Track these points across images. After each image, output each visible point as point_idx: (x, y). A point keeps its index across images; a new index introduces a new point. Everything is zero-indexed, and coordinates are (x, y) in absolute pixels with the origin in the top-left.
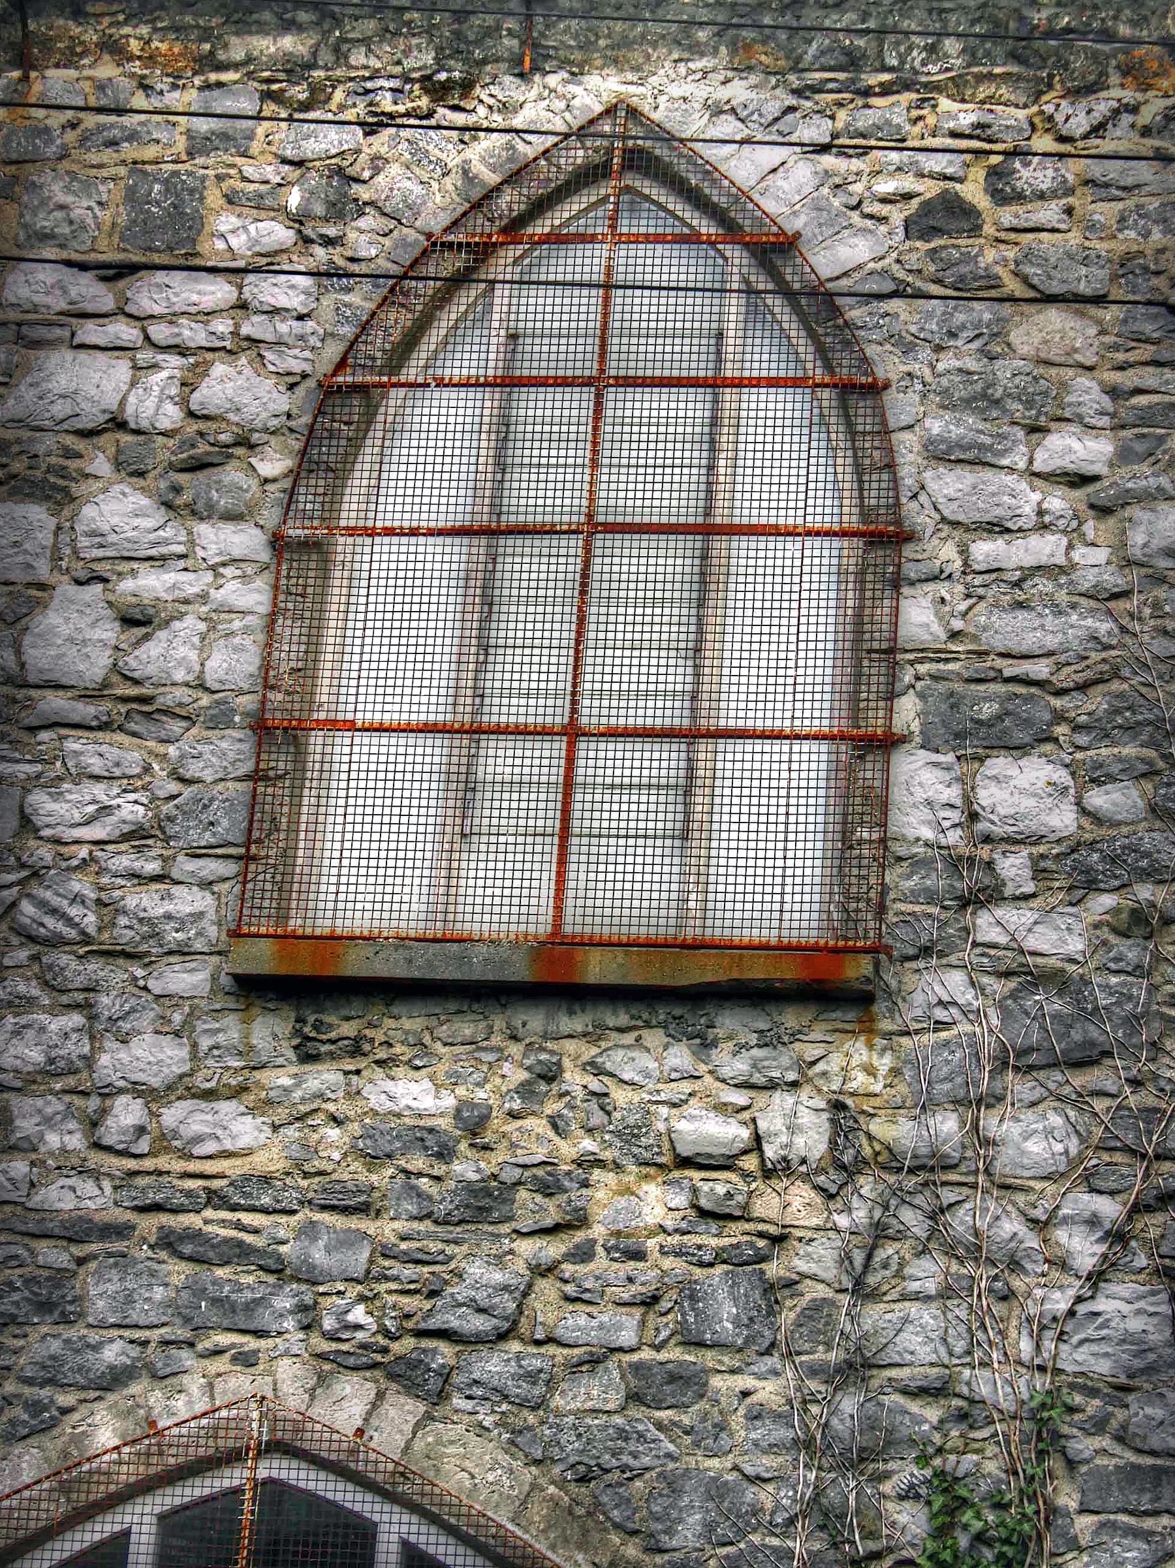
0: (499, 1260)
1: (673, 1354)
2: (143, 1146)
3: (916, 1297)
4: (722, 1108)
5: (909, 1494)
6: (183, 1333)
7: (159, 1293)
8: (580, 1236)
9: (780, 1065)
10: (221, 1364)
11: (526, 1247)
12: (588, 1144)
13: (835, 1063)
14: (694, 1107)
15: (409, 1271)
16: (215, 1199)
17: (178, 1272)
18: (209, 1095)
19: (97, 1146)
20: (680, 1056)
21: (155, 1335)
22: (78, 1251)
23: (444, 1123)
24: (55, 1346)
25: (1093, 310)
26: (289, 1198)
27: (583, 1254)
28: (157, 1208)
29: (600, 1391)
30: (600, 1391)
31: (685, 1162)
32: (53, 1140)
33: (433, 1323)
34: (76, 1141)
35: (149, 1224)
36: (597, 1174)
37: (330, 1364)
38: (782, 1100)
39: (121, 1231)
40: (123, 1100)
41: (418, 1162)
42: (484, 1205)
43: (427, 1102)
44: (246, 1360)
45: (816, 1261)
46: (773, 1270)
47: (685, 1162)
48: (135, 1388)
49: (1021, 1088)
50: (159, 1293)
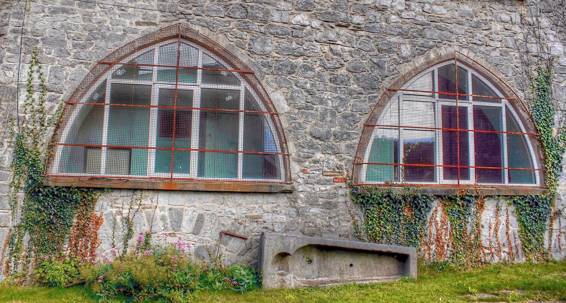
0: (481, 34)
1: (505, 49)
2: (430, 12)
3: (533, 43)
4: (507, 14)
5: (535, 70)
6: (440, 41)
7: (436, 34)
8: (490, 31)
9: (513, 9)
10: (446, 46)
11: (484, 32)
12: (490, 18)
13: (520, 9)
14: (503, 14)
15: (470, 34)
16: (442, 21)
17: (438, 31)
18: (438, 5)
19: (423, 11)
20: (501, 6)
21: (437, 41)
22: (424, 27)
23: (471, 13)
24: (423, 41)
25: (288, 195)
26: (452, 22)
27: (491, 33)
28: (434, 21)
29: (496, 53)
30: (496, 53)
31: (502, 21)
32: (417, 10)
33: (474, 42)
34: (421, 10)
35: (433, 24)
36: (492, 22)
37: (462, 47)
38: (514, 13)
39: (429, 25)
40: (427, 4)
41: (468, 18)
42: (477, 26)
43: (468, 9)
44: (450, 46)
45: (520, 37)
46: (515, 37)
47: (502, 21)
48: (435, 49)
49: (543, 15)
50: (436, 34)
